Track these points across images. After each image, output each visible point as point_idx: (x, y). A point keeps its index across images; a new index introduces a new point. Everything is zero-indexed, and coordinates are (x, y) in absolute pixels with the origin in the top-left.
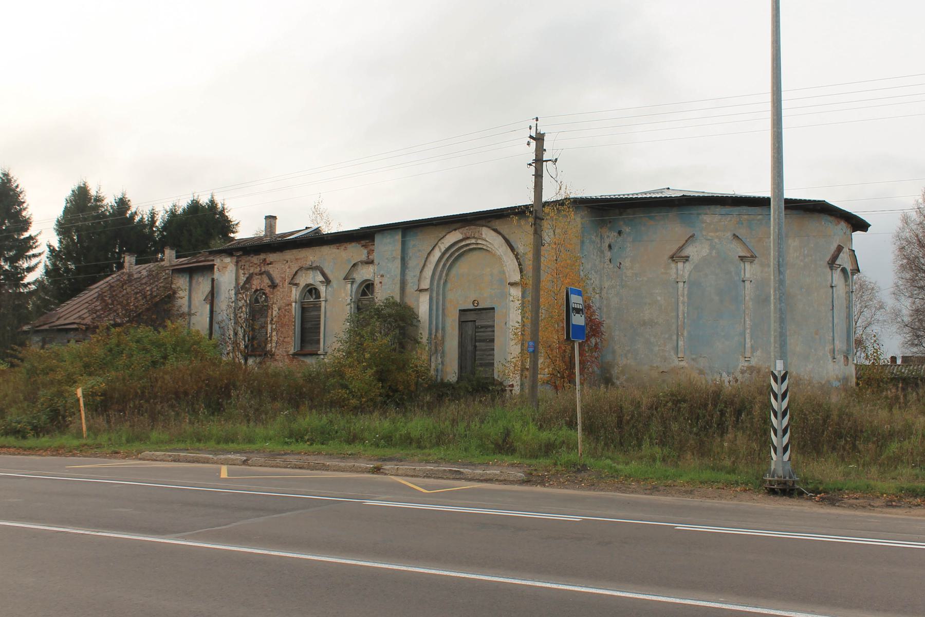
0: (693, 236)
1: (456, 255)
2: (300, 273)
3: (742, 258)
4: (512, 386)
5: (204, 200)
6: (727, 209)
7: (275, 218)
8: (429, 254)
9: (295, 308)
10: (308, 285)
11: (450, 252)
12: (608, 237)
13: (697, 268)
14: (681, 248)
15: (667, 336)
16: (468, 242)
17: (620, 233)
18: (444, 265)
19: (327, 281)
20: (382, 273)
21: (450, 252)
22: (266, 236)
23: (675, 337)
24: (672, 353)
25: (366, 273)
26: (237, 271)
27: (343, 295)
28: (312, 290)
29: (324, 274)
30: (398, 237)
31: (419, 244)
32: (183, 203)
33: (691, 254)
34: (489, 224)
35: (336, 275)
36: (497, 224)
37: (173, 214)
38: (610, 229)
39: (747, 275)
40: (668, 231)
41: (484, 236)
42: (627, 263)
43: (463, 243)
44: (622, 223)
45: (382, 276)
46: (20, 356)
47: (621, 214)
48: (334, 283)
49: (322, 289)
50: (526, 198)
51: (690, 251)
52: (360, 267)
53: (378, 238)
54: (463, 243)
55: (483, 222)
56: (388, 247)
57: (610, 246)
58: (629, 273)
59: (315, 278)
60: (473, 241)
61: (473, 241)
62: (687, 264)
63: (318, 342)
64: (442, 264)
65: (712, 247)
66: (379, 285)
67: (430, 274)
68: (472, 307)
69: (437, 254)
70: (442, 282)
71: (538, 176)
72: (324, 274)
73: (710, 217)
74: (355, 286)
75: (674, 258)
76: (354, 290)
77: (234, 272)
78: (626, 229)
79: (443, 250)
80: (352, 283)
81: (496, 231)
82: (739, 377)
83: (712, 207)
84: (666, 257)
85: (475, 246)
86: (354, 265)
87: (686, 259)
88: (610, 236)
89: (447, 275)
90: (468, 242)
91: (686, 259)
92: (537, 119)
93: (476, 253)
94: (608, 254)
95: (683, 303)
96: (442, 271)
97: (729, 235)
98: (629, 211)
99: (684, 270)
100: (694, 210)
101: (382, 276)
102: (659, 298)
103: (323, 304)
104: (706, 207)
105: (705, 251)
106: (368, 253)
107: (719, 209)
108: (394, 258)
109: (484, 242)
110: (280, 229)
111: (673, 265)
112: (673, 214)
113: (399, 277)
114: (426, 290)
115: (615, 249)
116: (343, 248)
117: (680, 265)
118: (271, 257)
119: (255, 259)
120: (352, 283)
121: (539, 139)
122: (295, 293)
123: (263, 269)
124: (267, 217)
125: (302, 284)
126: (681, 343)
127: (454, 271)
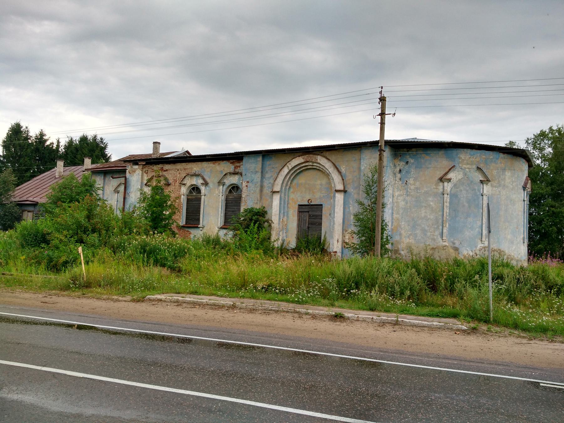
0: (454, 166)
1: (298, 172)
2: (187, 178)
3: (482, 182)
4: (336, 252)
5: (90, 135)
6: (474, 151)
7: (159, 143)
8: (281, 170)
9: (184, 199)
10: (192, 185)
11: (294, 170)
12: (399, 165)
13: (455, 185)
14: (446, 174)
15: (436, 226)
16: (307, 164)
17: (407, 163)
18: (290, 177)
19: (206, 184)
20: (248, 180)
21: (294, 170)
22: (154, 154)
23: (441, 227)
24: (439, 237)
25: (234, 180)
26: (142, 175)
27: (217, 192)
28: (195, 189)
29: (204, 179)
30: (260, 159)
31: (272, 163)
32: (76, 138)
33: (452, 178)
34: (322, 154)
35: (213, 181)
36: (327, 154)
37: (71, 142)
38: (400, 160)
39: (485, 192)
40: (438, 163)
41: (319, 161)
42: (411, 181)
43: (304, 165)
44: (408, 157)
45: (248, 182)
46: (17, 263)
47: (408, 151)
48: (211, 185)
49: (203, 189)
50: (377, 138)
51: (451, 175)
52: (228, 176)
53: (245, 160)
54: (304, 165)
55: (318, 153)
56: (248, 165)
57: (400, 171)
58: (412, 187)
59: (198, 182)
60: (311, 164)
61: (311, 164)
62: (450, 183)
63: (199, 220)
64: (288, 177)
65: (465, 174)
66: (245, 187)
67: (281, 182)
68: (306, 203)
69: (286, 170)
70: (288, 187)
71: (382, 123)
72: (204, 179)
73: (464, 155)
74: (225, 187)
75: (441, 180)
76: (224, 190)
77: (140, 174)
78: (411, 161)
79: (290, 168)
80: (223, 185)
81: (324, 157)
82: (478, 252)
83: (465, 150)
84: (437, 179)
85: (311, 167)
86: (226, 174)
87: (449, 180)
88: (401, 164)
89: (291, 183)
90: (307, 164)
91: (449, 180)
92: (382, 88)
93: (311, 171)
94: (399, 176)
95: (447, 207)
96: (288, 181)
97: (474, 167)
98: (413, 149)
99: (448, 186)
100: (455, 152)
101: (248, 182)
102: (432, 203)
103: (203, 197)
104: (455, 149)
105: (460, 176)
106: (235, 168)
107: (469, 151)
108: (256, 172)
109: (318, 165)
110: (162, 150)
111: (441, 184)
112: (442, 152)
113: (259, 183)
114: (278, 192)
115: (403, 173)
116: (217, 164)
117: (446, 184)
118: (167, 167)
119: (156, 167)
120: (223, 185)
121: (382, 100)
122: (184, 190)
123: (161, 174)
124: (154, 143)
125: (188, 184)
126: (445, 231)
127: (295, 181)
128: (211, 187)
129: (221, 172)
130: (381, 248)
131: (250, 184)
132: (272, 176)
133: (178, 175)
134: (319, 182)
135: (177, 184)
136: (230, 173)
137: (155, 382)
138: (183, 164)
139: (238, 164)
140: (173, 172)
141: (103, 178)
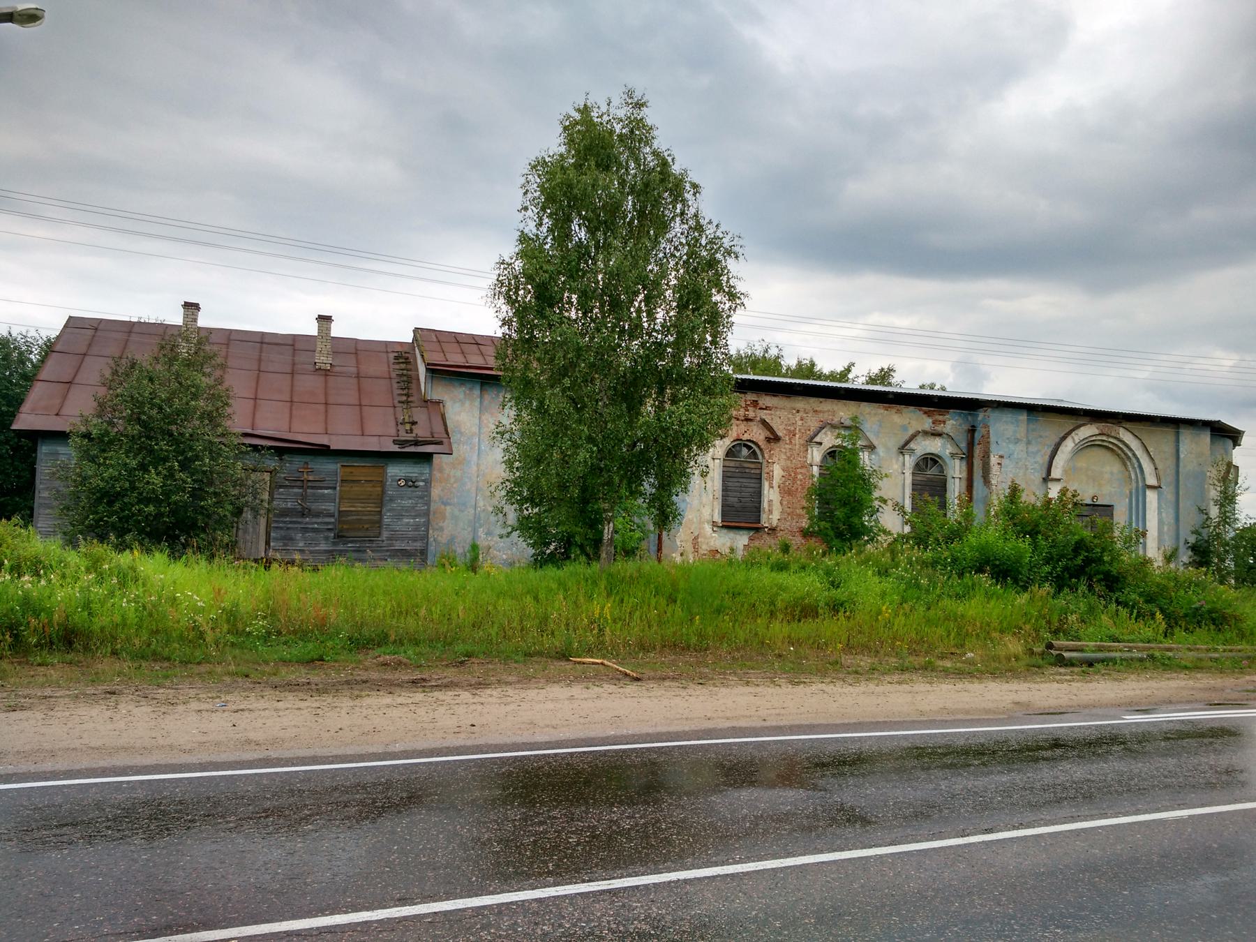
14: (907, 443)
45: (1001, 457)
48: (881, 450)
59: (758, 434)
68: (1089, 502)
111: (901, 458)
118: (766, 400)
128: (881, 454)
129: (904, 428)
130: (250, 445)
131: (1004, 462)
132: (1039, 451)
133: (800, 423)
134: (1108, 469)
135: (797, 440)
136: (926, 433)
137: (919, 645)
138: (812, 400)
139: (941, 418)
140: (784, 414)
141: (477, 403)
